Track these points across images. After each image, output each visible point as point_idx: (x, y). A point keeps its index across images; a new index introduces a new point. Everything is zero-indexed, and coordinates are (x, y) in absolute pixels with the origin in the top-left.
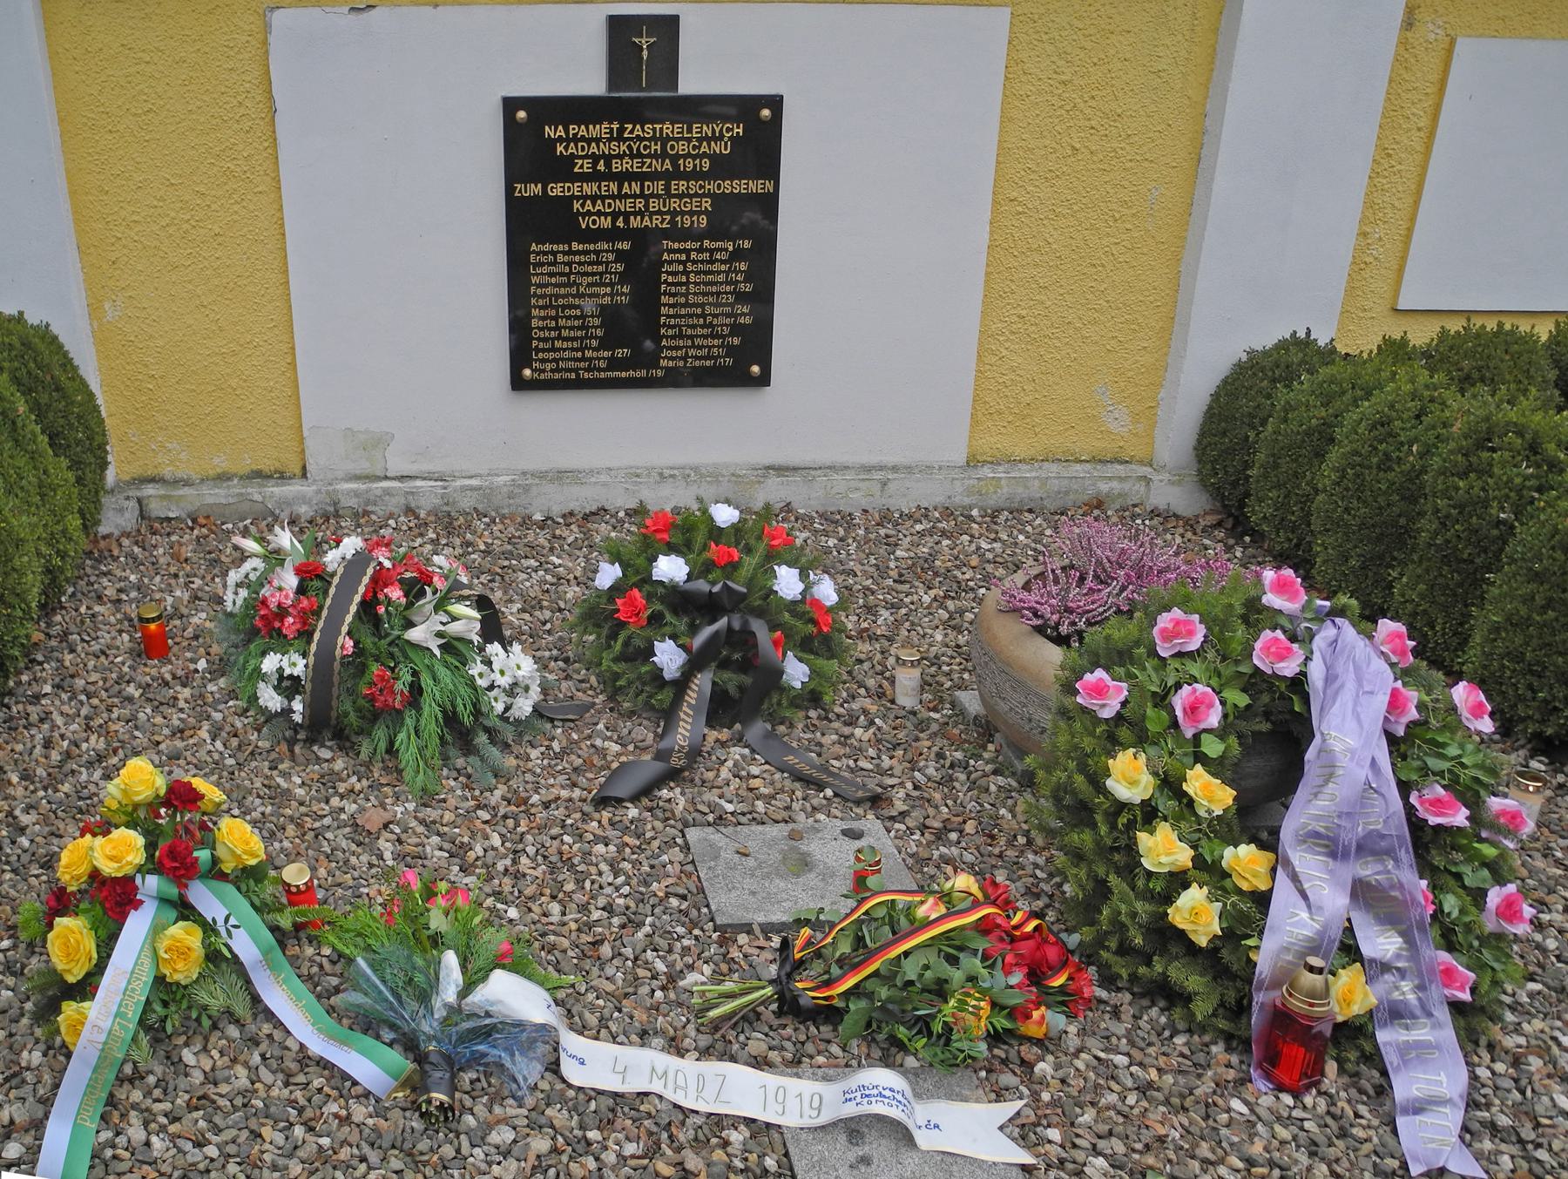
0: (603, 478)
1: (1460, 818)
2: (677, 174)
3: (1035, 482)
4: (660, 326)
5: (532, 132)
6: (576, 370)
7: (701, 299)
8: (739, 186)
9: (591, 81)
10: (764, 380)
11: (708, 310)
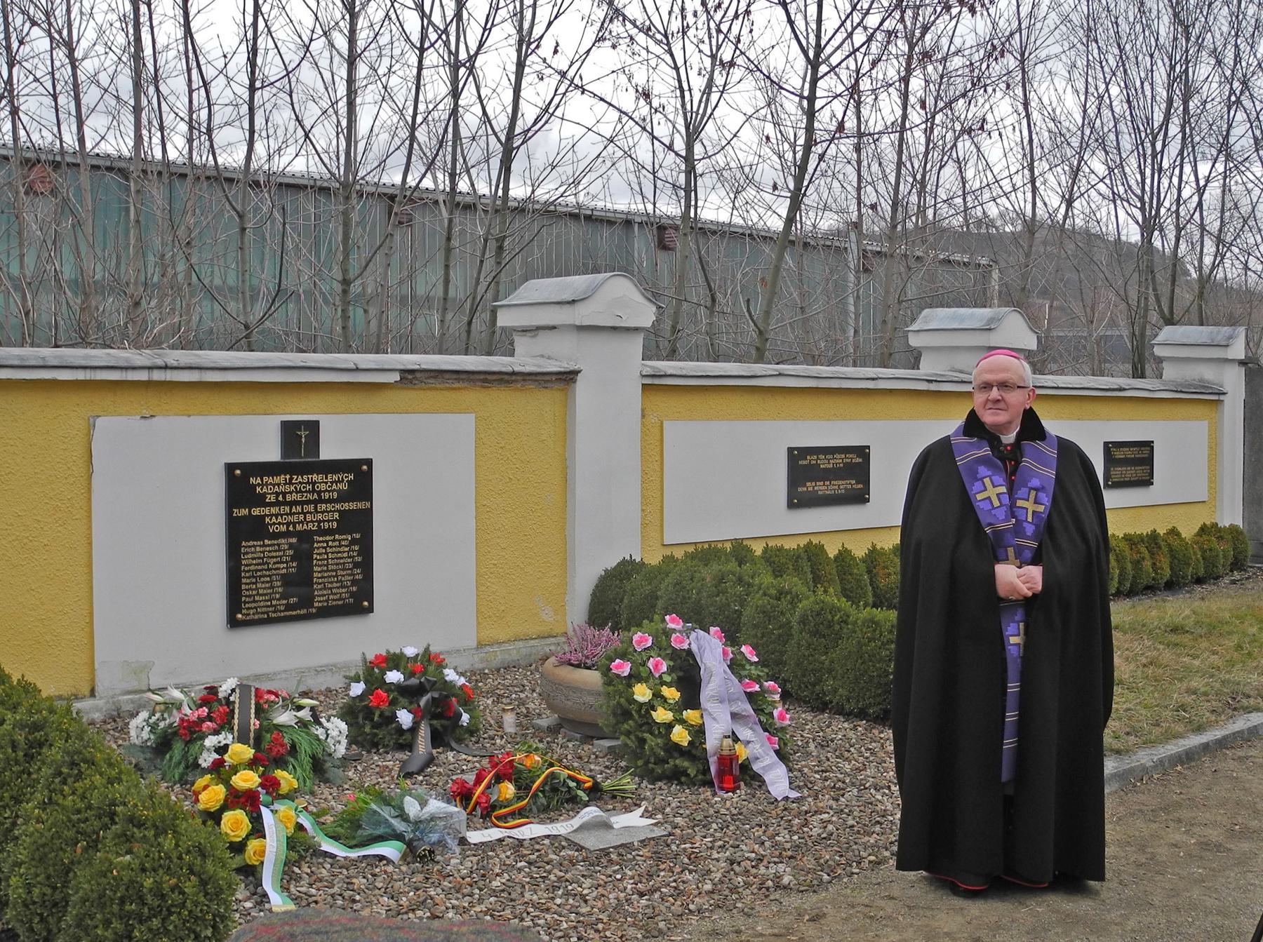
0: (284, 676)
1: (757, 688)
2: (321, 501)
3: (514, 652)
4: (313, 584)
5: (241, 483)
6: (267, 613)
7: (335, 567)
8: (352, 506)
9: (272, 454)
10: (370, 609)
11: (339, 573)
